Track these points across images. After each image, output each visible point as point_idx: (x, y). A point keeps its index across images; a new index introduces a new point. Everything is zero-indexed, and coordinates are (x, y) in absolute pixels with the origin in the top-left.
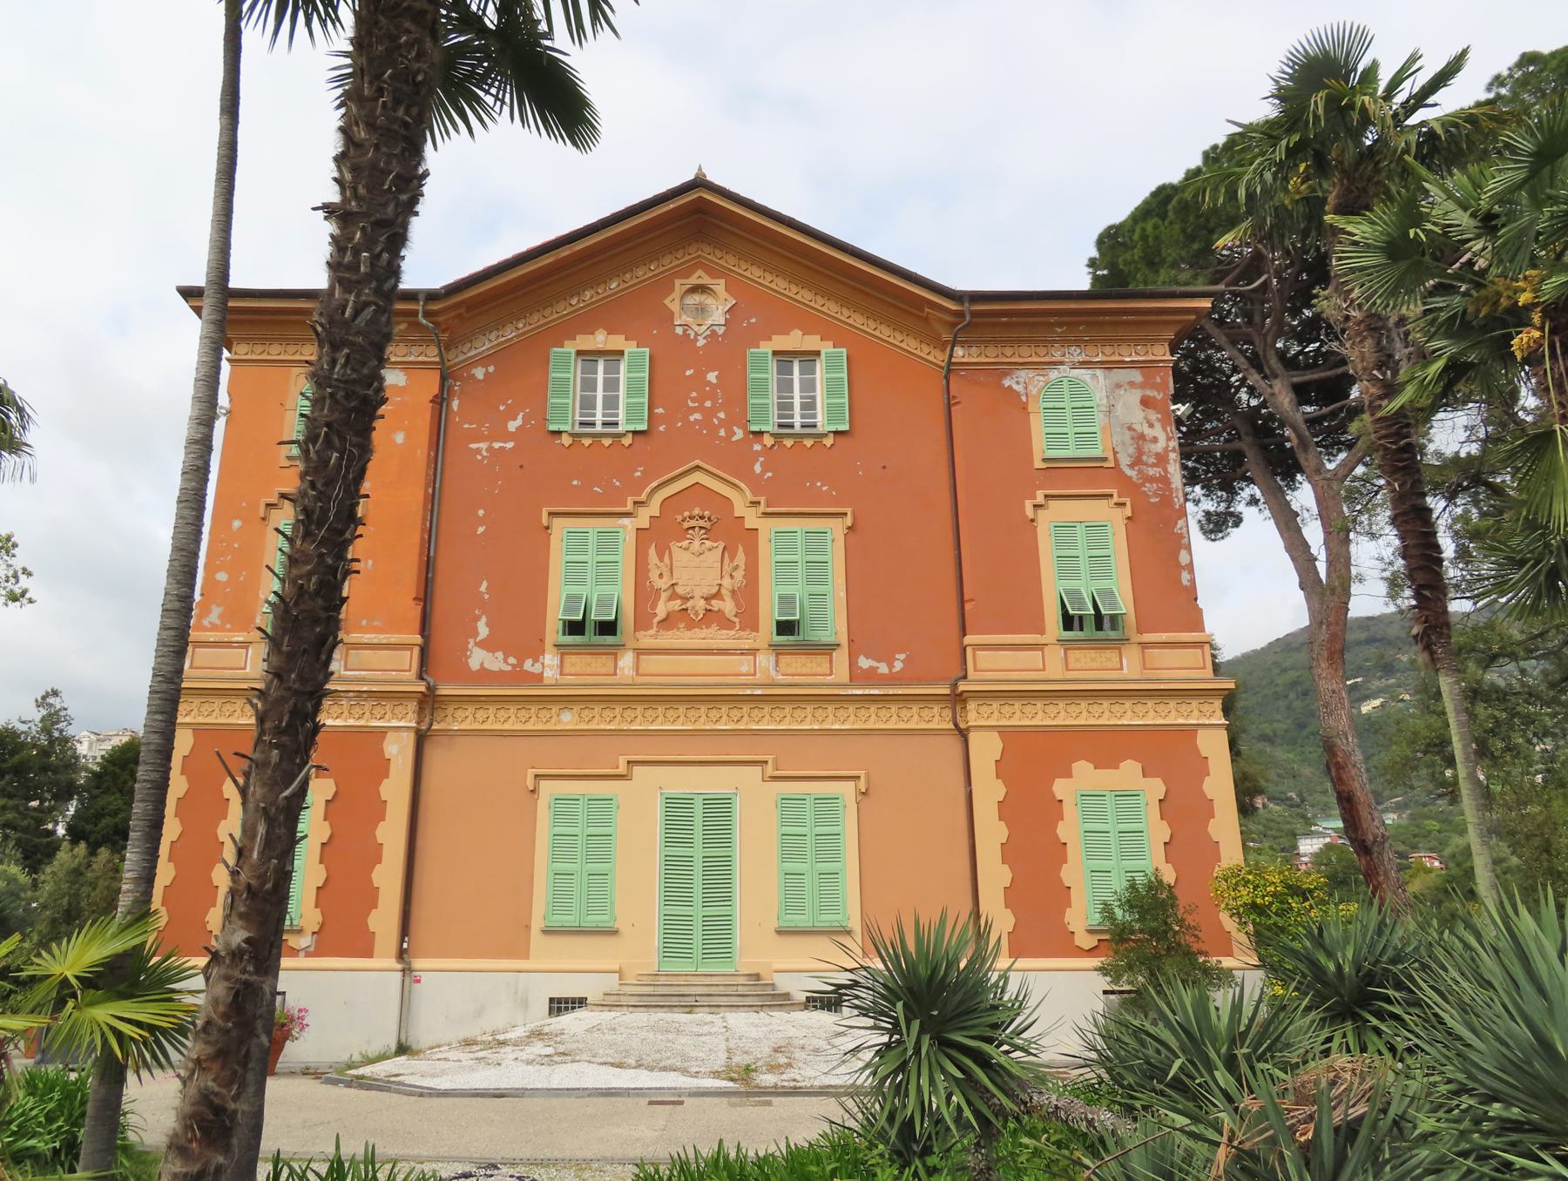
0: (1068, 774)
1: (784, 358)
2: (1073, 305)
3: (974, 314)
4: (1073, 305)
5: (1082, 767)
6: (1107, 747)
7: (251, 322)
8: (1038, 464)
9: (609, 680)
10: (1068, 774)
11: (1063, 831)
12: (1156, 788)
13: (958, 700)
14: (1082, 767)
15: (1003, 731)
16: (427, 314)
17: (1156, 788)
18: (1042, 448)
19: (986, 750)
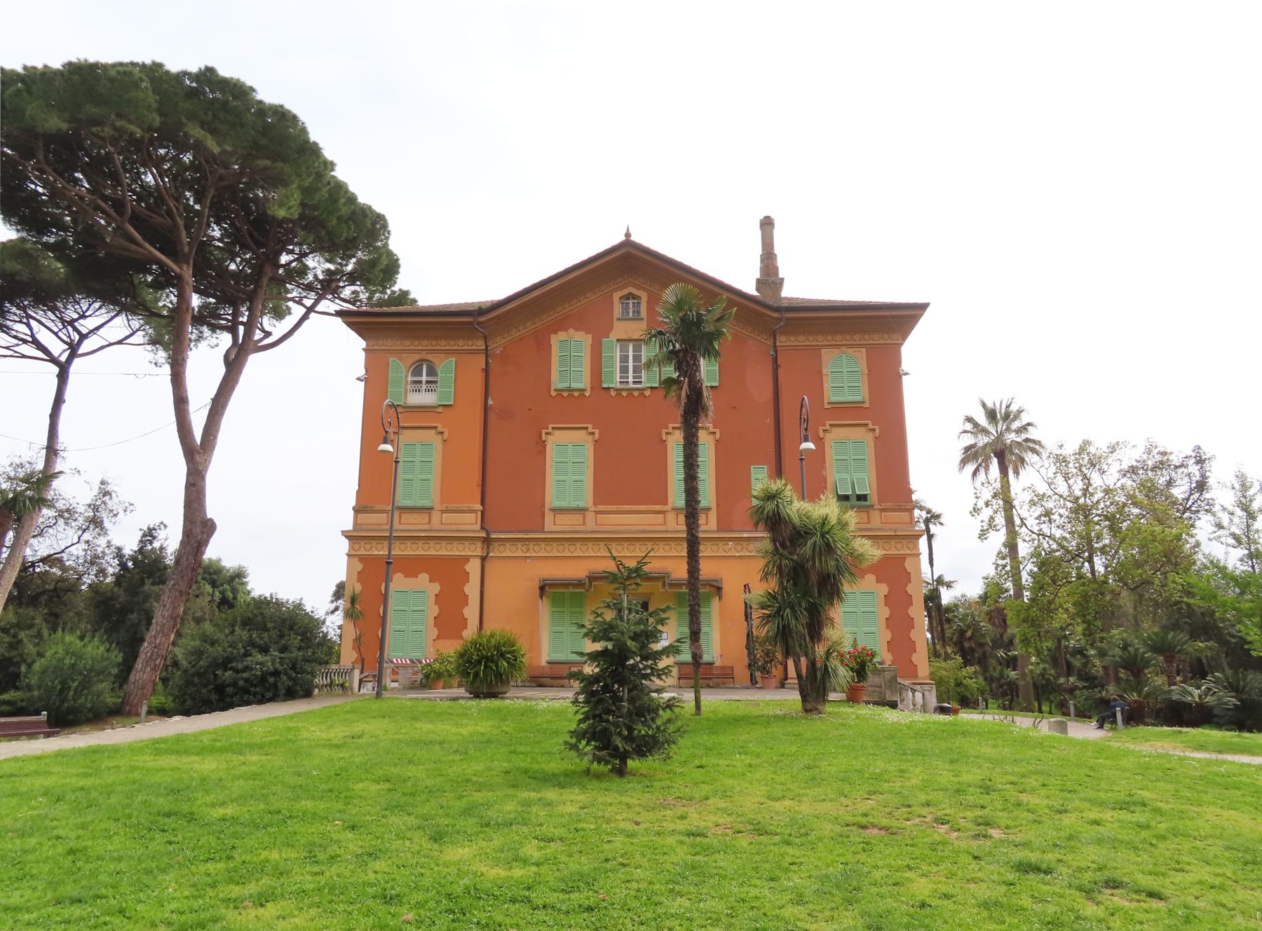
6: (412, 567)
9: (581, 528)
17: (436, 588)
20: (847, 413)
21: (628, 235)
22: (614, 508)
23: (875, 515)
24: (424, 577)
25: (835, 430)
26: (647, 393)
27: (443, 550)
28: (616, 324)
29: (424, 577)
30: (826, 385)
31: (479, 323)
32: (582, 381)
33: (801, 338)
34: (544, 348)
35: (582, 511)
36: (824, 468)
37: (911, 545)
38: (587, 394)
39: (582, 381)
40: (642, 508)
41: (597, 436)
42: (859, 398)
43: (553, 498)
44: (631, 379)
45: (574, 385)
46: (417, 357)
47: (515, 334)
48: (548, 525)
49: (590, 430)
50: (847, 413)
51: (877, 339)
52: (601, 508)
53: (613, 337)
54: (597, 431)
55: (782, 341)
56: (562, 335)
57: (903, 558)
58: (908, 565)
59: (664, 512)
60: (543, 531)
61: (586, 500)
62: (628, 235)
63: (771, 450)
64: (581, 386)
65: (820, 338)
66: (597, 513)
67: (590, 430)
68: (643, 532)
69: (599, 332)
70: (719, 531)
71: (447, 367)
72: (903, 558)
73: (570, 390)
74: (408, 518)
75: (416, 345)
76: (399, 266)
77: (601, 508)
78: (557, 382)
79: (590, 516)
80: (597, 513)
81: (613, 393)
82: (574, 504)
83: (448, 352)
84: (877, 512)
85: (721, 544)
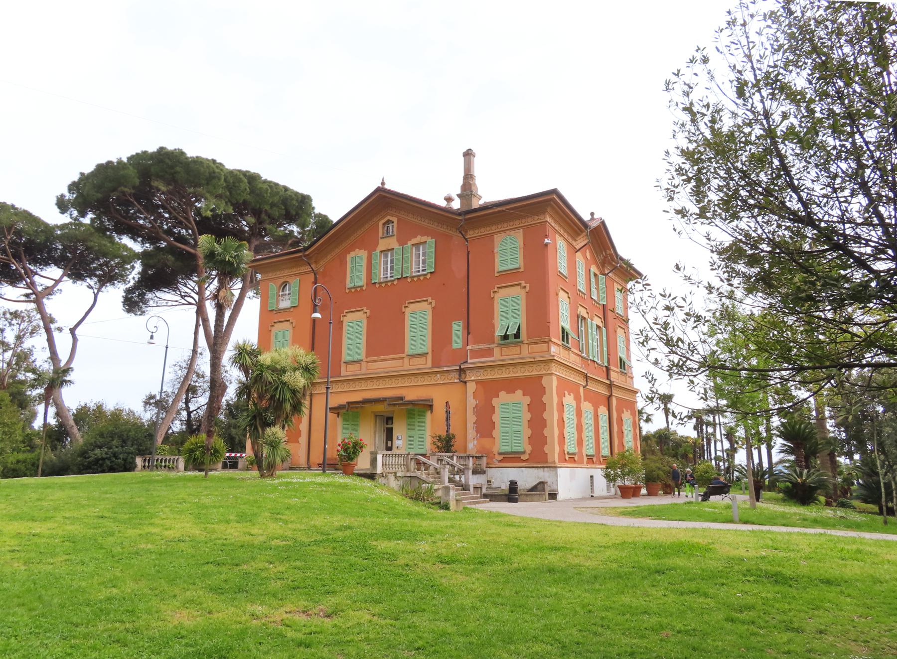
0: (498, 396)
1: (417, 245)
2: (450, 215)
3: (466, 220)
4: (450, 215)
5: (502, 394)
6: (510, 385)
7: (570, 225)
8: (496, 275)
9: (358, 372)
10: (498, 396)
11: (495, 418)
12: (527, 400)
13: (462, 371)
14: (502, 394)
15: (477, 382)
16: (305, 256)
17: (527, 400)
18: (500, 267)
19: (471, 387)
20: (510, 277)
21: (383, 183)
22: (376, 358)
23: (525, 348)
24: (519, 393)
25: (349, 315)
26: (428, 276)
27: (527, 372)
28: (380, 241)
29: (519, 393)
30: (496, 260)
31: (305, 256)
32: (362, 282)
33: (482, 230)
34: (343, 263)
35: (359, 362)
36: (493, 318)
37: (546, 367)
38: (364, 288)
39: (362, 282)
40: (382, 357)
41: (528, 289)
42: (516, 266)
43: (345, 357)
44: (389, 275)
45: (357, 284)
46: (282, 280)
47: (329, 257)
48: (343, 373)
49: (523, 284)
50: (510, 277)
51: (530, 221)
52: (370, 359)
53: (378, 251)
54: (528, 286)
55: (471, 234)
56: (352, 254)
57: (540, 377)
58: (544, 381)
59: (402, 358)
60: (340, 376)
61: (362, 356)
62: (383, 183)
63: (465, 310)
64: (360, 284)
65: (494, 227)
66: (368, 362)
67: (523, 284)
68: (385, 372)
69: (370, 247)
70: (433, 367)
71: (295, 282)
72: (540, 377)
73: (355, 287)
74: (352, 368)
75: (278, 274)
76: (325, 216)
77: (370, 359)
78: (349, 284)
79: (364, 364)
80: (368, 362)
81: (409, 280)
82: (356, 358)
83: (296, 275)
84: (526, 346)
85: (433, 376)
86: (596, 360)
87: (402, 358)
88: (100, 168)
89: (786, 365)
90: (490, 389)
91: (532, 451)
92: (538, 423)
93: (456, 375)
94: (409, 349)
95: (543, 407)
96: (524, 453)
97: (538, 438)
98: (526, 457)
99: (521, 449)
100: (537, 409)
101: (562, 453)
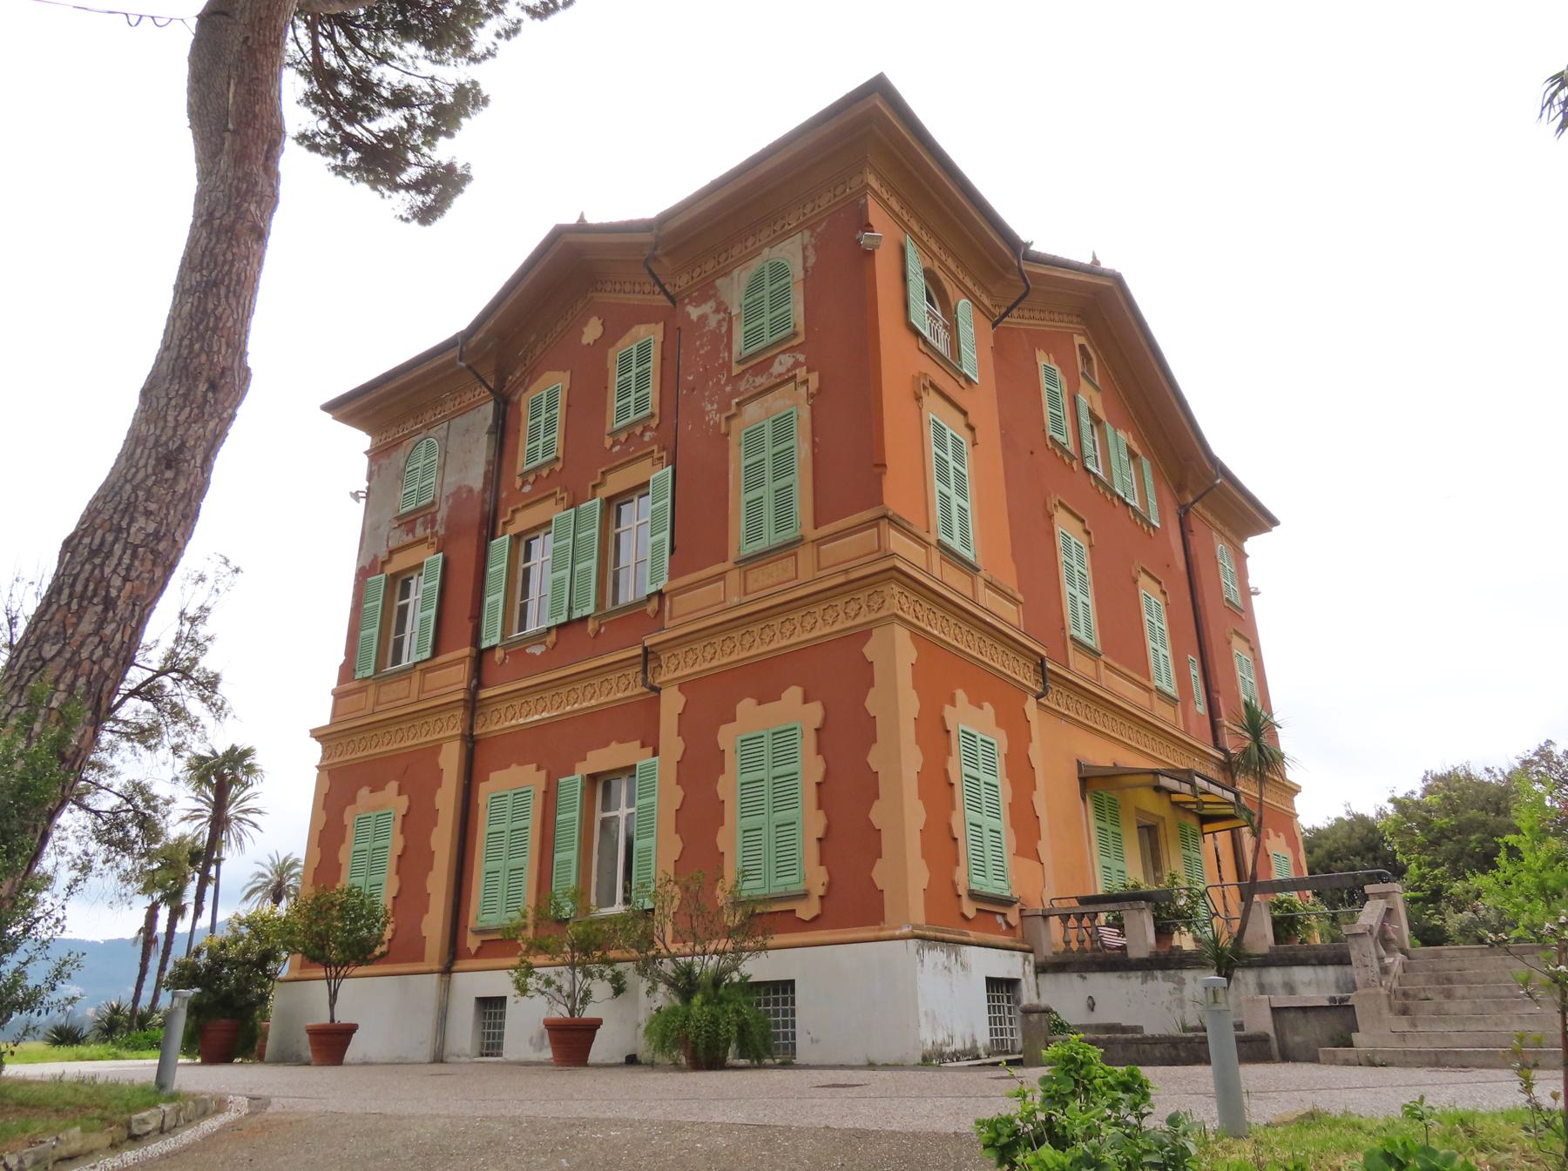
5: (746, 707)
6: (762, 679)
24: (794, 693)
52: (825, 530)
66: (819, 542)
86: (955, 544)
87: (721, 576)
88: (246, 374)
89: (605, 927)
90: (714, 698)
91: (830, 886)
92: (848, 795)
93: (633, 672)
94: (741, 544)
95: (867, 731)
96: (805, 895)
97: (850, 841)
98: (806, 911)
99: (791, 883)
100: (847, 741)
101: (943, 892)
